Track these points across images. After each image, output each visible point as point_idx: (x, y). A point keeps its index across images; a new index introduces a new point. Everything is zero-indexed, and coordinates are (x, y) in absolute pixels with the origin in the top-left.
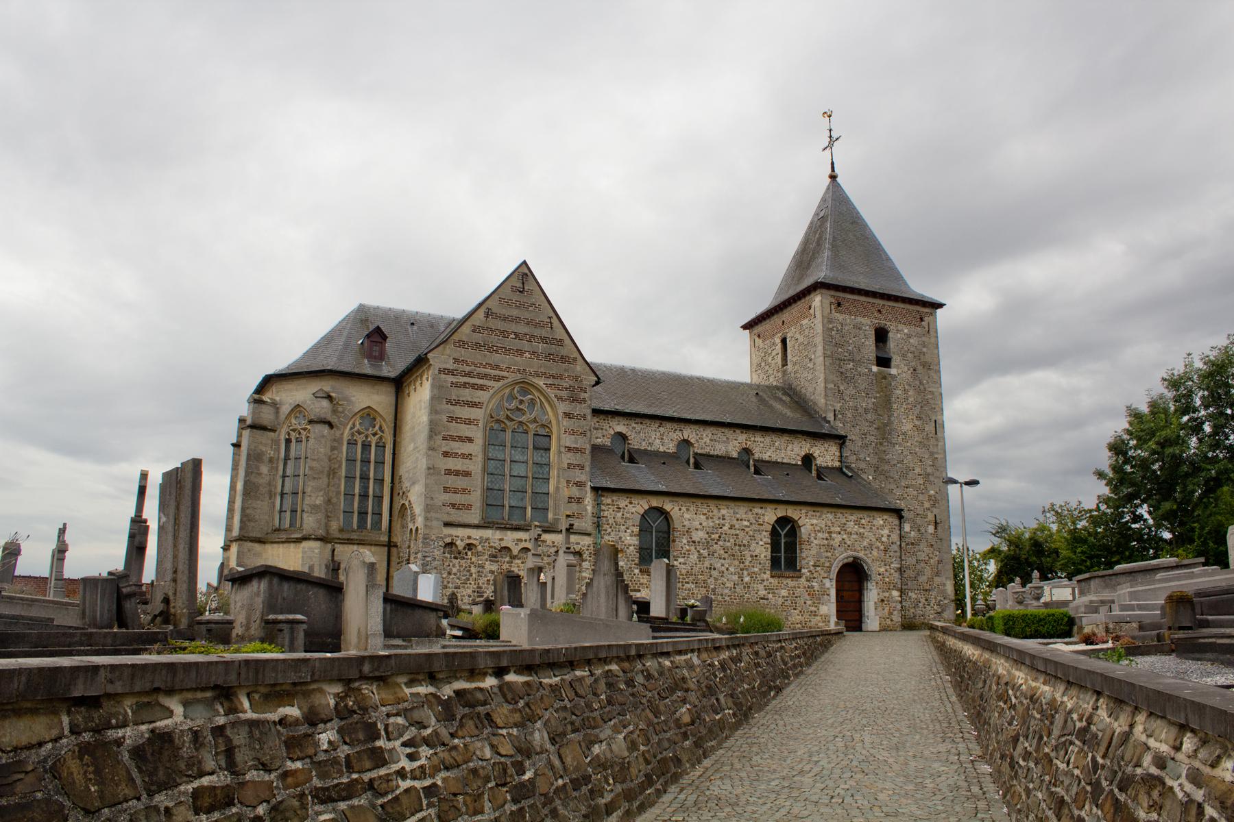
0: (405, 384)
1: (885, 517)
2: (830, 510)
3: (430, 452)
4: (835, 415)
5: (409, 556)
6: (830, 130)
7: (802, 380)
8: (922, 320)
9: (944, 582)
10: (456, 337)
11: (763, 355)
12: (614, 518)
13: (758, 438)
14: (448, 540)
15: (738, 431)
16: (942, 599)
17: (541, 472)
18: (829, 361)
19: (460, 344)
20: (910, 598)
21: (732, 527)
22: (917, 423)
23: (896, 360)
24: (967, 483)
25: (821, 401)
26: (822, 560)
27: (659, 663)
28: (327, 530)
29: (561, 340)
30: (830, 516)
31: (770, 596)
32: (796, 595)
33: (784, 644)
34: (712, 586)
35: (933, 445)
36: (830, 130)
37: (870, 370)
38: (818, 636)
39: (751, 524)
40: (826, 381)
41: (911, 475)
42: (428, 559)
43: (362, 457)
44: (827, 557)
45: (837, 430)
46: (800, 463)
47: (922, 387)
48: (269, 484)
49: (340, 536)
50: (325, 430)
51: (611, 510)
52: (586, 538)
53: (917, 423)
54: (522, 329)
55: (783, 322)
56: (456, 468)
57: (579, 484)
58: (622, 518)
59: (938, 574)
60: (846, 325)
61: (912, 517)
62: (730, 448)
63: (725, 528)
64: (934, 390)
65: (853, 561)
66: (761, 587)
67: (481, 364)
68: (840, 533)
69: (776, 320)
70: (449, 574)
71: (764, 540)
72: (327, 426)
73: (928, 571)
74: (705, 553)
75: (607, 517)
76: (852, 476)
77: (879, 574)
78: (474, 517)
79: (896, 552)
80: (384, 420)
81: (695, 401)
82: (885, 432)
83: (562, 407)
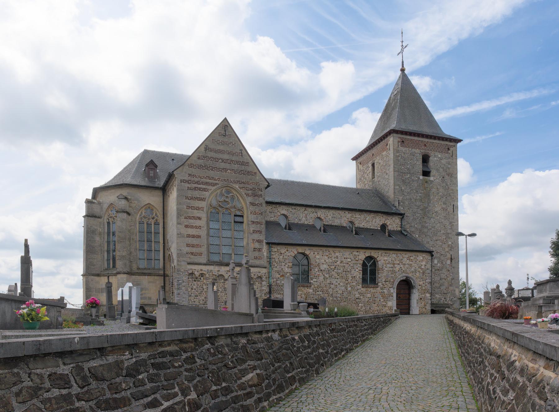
1: (424, 255)
7: (382, 185)
8: (449, 149)
12: (279, 259)
13: (357, 215)
14: (190, 272)
15: (347, 212)
17: (239, 235)
18: (396, 174)
19: (191, 166)
21: (341, 262)
22: (444, 206)
23: (433, 172)
24: (470, 235)
26: (389, 279)
28: (131, 269)
29: (248, 163)
30: (394, 256)
31: (362, 297)
32: (375, 296)
34: (331, 293)
37: (419, 178)
39: (352, 260)
40: (395, 185)
42: (180, 282)
43: (147, 230)
44: (392, 277)
45: (400, 211)
46: (379, 229)
49: (138, 272)
51: (277, 255)
52: (264, 269)
53: (444, 206)
54: (226, 157)
55: (373, 154)
57: (259, 241)
58: (283, 259)
59: (451, 286)
61: (439, 256)
62: (342, 221)
64: (454, 188)
66: (357, 293)
67: (204, 177)
68: (399, 264)
69: (369, 153)
70: (192, 289)
71: (359, 268)
72: (125, 214)
73: (446, 284)
74: (327, 276)
75: (274, 258)
76: (407, 235)
78: (204, 260)
80: (158, 211)
82: (425, 212)
83: (249, 199)
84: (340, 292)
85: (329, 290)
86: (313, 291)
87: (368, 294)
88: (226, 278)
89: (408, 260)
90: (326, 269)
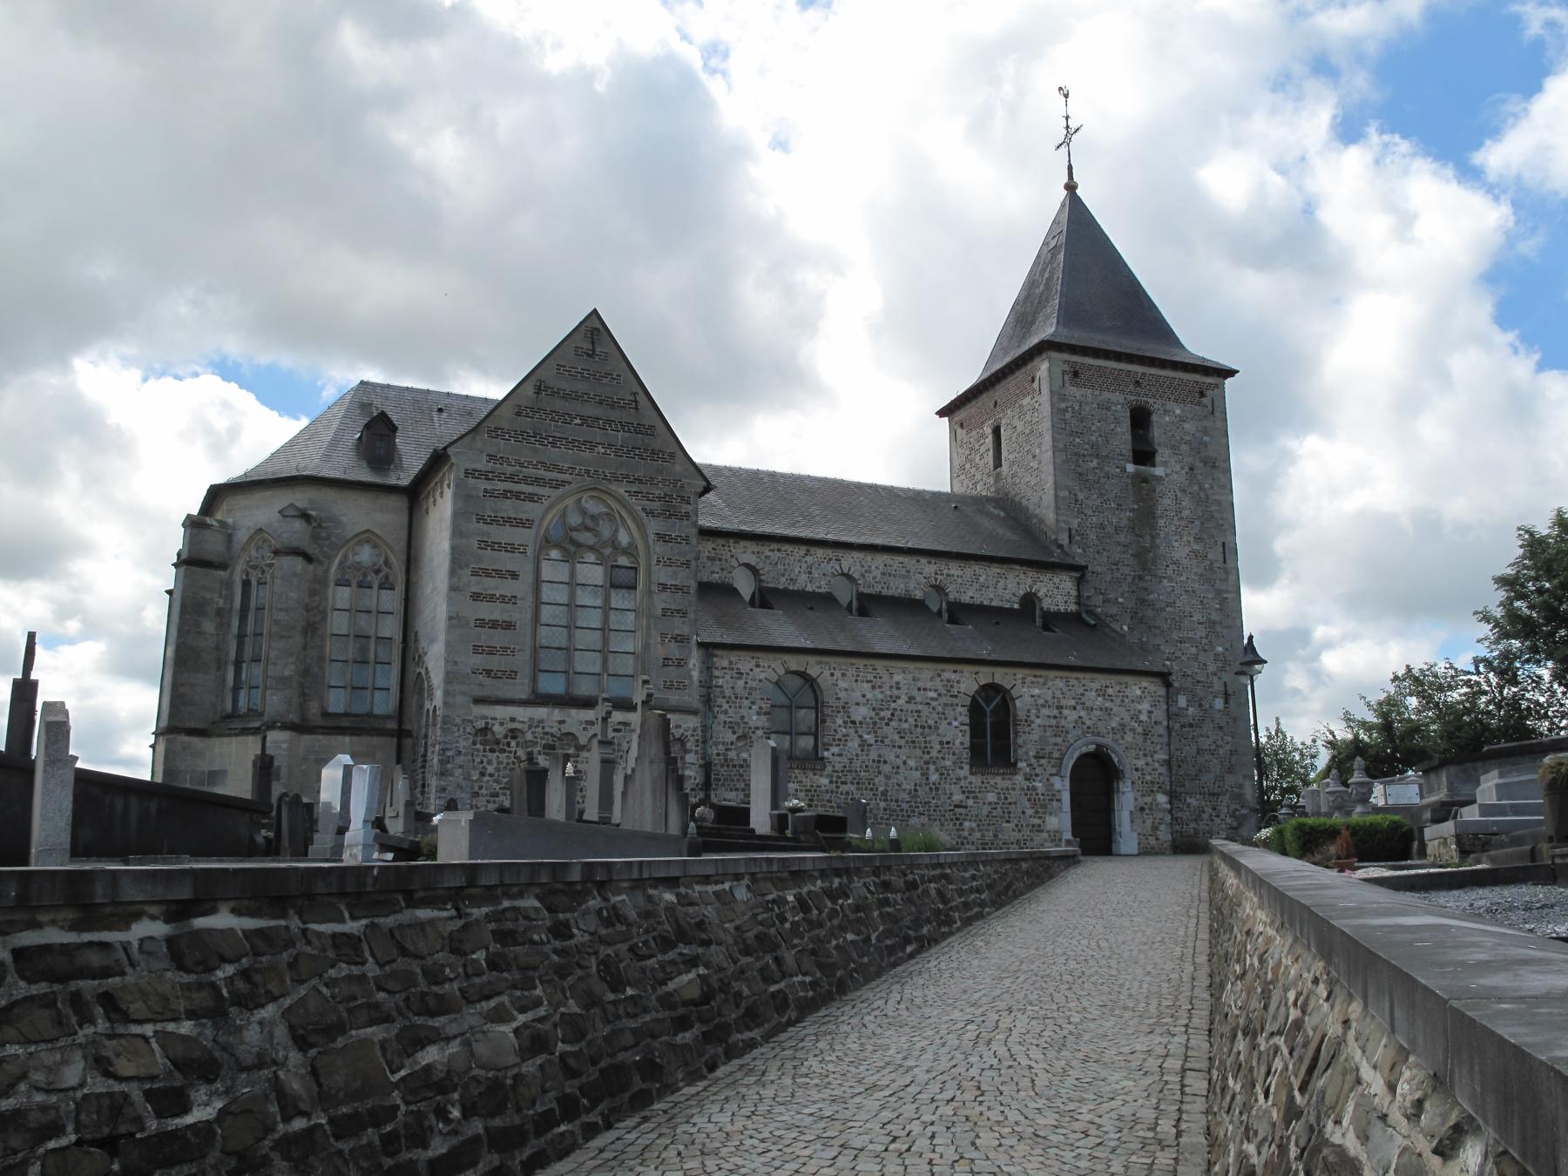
0: (422, 496)
1: (1144, 684)
2: (1059, 673)
3: (453, 594)
4: (1070, 535)
5: (426, 750)
6: (1067, 118)
8: (1202, 394)
9: (1241, 781)
10: (490, 424)
11: (967, 452)
14: (480, 724)
15: (924, 561)
16: (1239, 808)
20: (1189, 805)
21: (911, 699)
22: (1196, 547)
23: (1163, 454)
25: (1050, 516)
26: (1048, 749)
27: (650, 899)
29: (652, 427)
31: (970, 802)
33: (948, 871)
34: (881, 789)
35: (1221, 580)
36: (1067, 118)
38: (1025, 860)
39: (940, 695)
40: (1057, 486)
41: (1186, 622)
42: (449, 753)
44: (1056, 744)
45: (1073, 558)
47: (1202, 495)
48: (217, 648)
50: (298, 564)
51: (728, 677)
52: (691, 717)
53: (1196, 547)
54: (591, 410)
55: (996, 403)
56: (493, 617)
57: (680, 639)
58: (745, 688)
59: (1231, 770)
60: (1087, 404)
62: (912, 585)
63: (900, 702)
65: (1096, 750)
66: (955, 789)
68: (1075, 708)
69: (986, 399)
70: (482, 774)
75: (722, 687)
76: (1095, 625)
77: (1137, 770)
79: (1160, 736)
81: (861, 519)
82: (1146, 560)
83: (654, 526)
84: (908, 787)
85: (877, 780)
86: (831, 782)
87: (991, 794)
88: (582, 743)
89: (1099, 695)
90: (868, 719)
